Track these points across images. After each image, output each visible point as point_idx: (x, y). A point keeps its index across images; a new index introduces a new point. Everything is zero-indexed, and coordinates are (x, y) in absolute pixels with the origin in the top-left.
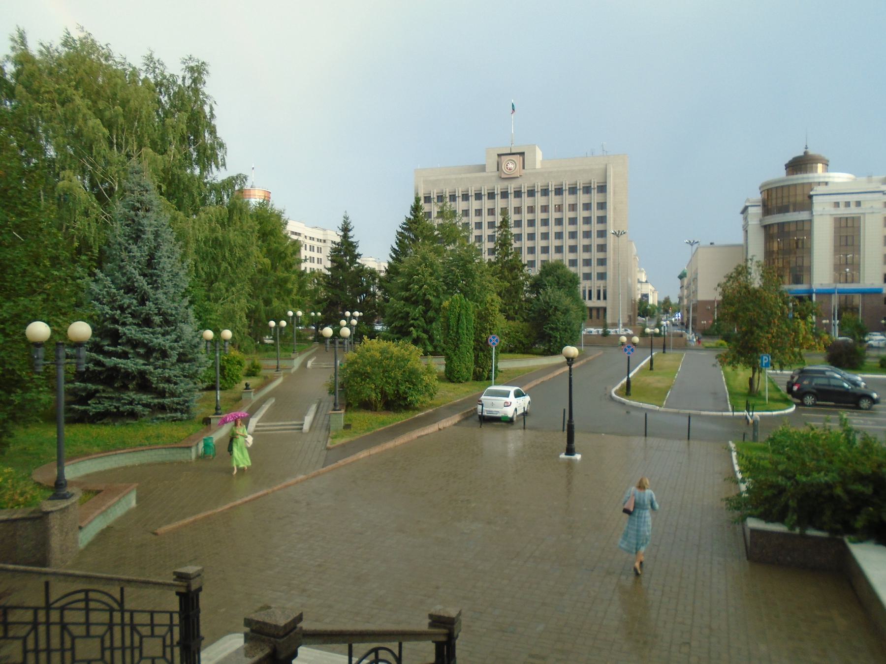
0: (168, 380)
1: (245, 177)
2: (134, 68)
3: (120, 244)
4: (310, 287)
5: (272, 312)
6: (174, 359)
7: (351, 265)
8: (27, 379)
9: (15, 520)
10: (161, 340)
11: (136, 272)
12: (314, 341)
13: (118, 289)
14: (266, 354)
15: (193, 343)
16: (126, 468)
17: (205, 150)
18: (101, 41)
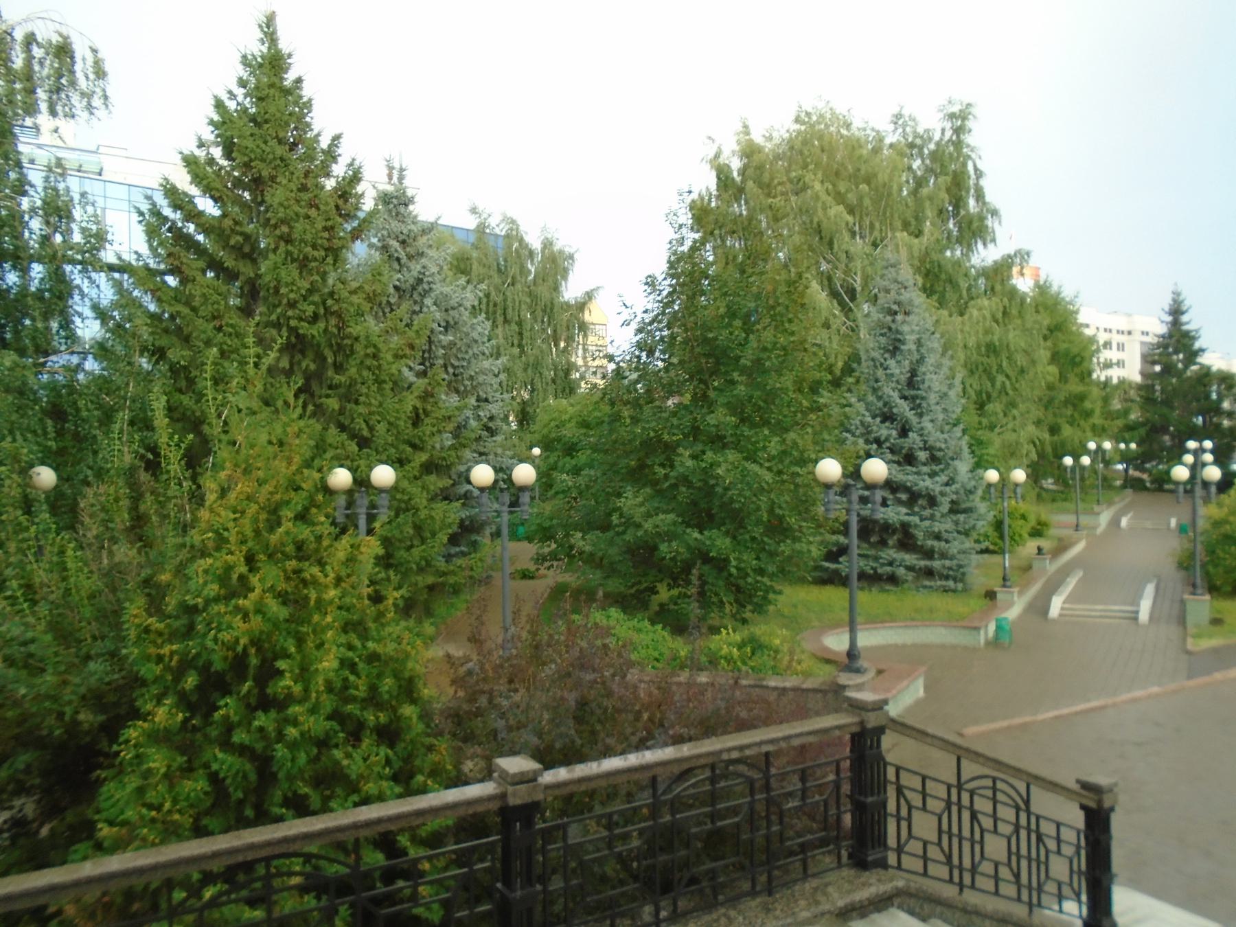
0: (938, 537)
1: (1028, 254)
2: (878, 132)
3: (873, 360)
4: (1116, 405)
5: (1063, 444)
6: (945, 508)
7: (1186, 367)
8: (796, 527)
9: (808, 690)
10: (928, 483)
11: (896, 395)
12: (1124, 487)
13: (874, 417)
14: (1055, 505)
15: (968, 488)
16: (896, 646)
17: (971, 222)
18: (841, 109)
